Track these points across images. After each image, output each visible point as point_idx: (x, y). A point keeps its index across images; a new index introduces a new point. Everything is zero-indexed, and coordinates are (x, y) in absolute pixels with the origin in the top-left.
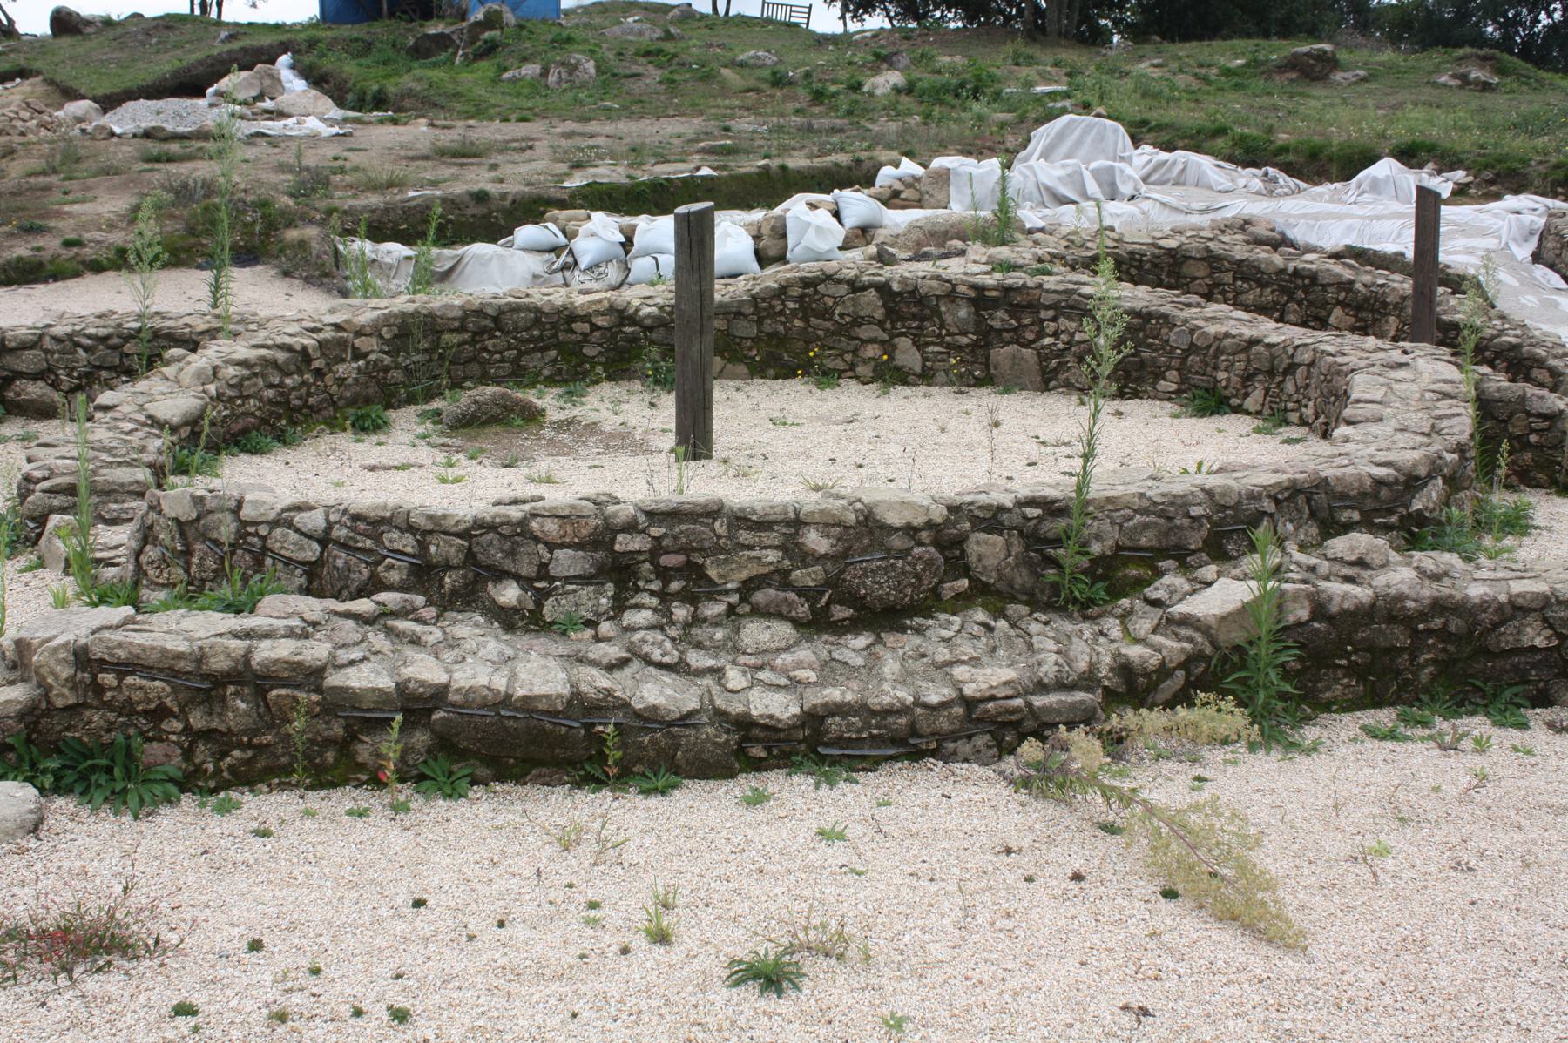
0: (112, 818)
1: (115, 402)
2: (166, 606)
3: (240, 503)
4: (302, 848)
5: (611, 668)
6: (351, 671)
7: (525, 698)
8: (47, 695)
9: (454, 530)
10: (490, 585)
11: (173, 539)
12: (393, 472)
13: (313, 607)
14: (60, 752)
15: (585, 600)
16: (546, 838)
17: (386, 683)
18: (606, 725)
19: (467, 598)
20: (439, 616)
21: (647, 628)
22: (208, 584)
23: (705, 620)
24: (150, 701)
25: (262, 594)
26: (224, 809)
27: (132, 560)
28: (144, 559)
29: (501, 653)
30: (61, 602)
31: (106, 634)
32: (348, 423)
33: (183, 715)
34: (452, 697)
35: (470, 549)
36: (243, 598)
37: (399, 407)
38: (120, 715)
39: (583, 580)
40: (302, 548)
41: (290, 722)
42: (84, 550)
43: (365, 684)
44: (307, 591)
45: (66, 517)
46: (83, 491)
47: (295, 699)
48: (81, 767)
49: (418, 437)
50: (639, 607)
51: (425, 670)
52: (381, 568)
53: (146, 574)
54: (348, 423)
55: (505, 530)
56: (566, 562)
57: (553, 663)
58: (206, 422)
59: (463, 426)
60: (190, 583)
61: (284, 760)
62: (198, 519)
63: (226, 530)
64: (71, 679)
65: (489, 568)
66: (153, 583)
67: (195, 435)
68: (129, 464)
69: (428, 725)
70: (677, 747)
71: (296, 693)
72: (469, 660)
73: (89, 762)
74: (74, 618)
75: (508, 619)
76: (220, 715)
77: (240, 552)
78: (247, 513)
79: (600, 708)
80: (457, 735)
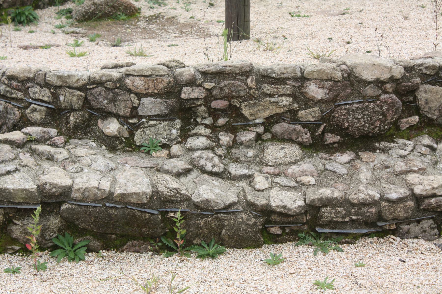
5: (178, 175)
6: (7, 178)
7: (122, 195)
9: (75, 85)
10: (100, 121)
12: (39, 50)
15: (162, 131)
16: (135, 287)
17: (31, 186)
18: (175, 212)
19: (85, 129)
20: (66, 142)
21: (203, 149)
23: (241, 144)
29: (107, 166)
34: (74, 195)
35: (86, 98)
37: (44, 8)
39: (161, 117)
49: (57, 27)
50: (197, 135)
51: (56, 177)
52: (28, 111)
55: (109, 85)
57: (140, 172)
59: (86, 20)
69: (58, 213)
70: (222, 227)
72: (86, 170)
75: (111, 144)
79: (172, 201)
80: (78, 219)
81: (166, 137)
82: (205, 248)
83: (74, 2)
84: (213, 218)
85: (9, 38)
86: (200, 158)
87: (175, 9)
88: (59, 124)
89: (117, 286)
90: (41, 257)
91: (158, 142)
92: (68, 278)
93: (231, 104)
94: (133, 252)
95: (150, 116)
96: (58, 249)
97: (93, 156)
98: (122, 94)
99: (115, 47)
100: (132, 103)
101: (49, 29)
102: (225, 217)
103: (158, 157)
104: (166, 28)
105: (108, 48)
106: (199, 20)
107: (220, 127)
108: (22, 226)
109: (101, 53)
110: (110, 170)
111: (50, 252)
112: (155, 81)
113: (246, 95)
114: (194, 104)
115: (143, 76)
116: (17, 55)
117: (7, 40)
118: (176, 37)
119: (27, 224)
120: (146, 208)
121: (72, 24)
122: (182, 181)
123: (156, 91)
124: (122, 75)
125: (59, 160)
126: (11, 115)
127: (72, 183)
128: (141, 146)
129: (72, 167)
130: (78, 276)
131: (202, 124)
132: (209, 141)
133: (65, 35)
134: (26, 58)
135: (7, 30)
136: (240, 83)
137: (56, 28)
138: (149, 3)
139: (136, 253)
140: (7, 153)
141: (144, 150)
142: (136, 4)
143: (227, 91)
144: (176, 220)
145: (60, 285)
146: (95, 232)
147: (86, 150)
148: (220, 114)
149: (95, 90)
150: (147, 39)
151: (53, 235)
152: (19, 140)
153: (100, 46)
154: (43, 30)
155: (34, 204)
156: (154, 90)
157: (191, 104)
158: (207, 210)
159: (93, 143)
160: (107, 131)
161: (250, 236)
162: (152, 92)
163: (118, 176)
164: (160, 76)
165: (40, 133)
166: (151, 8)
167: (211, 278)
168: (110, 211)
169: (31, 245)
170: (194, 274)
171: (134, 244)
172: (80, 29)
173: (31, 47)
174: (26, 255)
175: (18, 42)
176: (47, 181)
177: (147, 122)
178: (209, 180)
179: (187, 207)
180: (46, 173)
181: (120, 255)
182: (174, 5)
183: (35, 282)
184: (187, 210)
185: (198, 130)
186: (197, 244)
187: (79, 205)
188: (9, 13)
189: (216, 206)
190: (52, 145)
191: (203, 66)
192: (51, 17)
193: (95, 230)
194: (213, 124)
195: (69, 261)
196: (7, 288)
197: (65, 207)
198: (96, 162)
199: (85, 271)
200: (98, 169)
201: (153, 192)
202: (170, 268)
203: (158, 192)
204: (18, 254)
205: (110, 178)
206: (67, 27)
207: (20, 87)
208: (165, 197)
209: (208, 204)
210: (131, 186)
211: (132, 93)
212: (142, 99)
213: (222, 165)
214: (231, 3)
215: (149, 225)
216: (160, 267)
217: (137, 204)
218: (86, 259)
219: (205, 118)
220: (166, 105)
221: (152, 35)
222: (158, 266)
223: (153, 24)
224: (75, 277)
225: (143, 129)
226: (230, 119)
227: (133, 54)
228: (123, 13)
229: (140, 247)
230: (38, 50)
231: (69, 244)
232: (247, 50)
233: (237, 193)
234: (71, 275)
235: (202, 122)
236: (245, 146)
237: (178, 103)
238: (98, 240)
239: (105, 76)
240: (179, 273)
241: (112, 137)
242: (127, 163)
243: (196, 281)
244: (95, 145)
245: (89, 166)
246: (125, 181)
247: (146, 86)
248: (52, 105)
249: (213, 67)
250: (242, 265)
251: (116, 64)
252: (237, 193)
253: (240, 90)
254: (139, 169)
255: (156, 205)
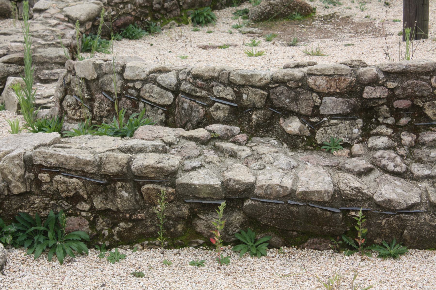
0: (47, 263)
1: (46, 7)
2: (78, 133)
3: (123, 68)
4: (162, 285)
5: (360, 174)
6: (193, 173)
7: (304, 193)
8: (8, 186)
9: (258, 84)
10: (281, 120)
11: (83, 91)
12: (218, 50)
13: (169, 133)
14: (16, 221)
15: (343, 130)
16: (317, 284)
17: (215, 181)
18: (356, 211)
19: (267, 128)
20: (248, 140)
21: (384, 149)
22: (104, 119)
23: (424, 144)
24: (70, 191)
25: (138, 125)
26: (115, 259)
27: (58, 104)
28: (65, 104)
29: (289, 163)
30: (16, 130)
31: (43, 149)
32: (190, 18)
33: (89, 200)
34: (257, 191)
35: (268, 97)
36: (126, 127)
37: (221, 9)
38: (52, 199)
39: (343, 117)
40: (162, 96)
41: (155, 205)
42: (29, 98)
43: (202, 182)
44: (165, 124)
45: (18, 79)
46: (28, 61)
47: (159, 191)
48: (28, 231)
49: (233, 27)
50: (379, 134)
51: (240, 174)
52: (212, 109)
53: (66, 113)
54: (190, 18)
55: (292, 84)
56: (331, 105)
57: (322, 171)
58: (102, 19)
59: (262, 20)
60: (93, 119)
61: (151, 229)
62: (98, 78)
63: (115, 86)
64: (22, 177)
65: (280, 109)
66: (71, 118)
67: (95, 27)
68: (55, 45)
69: (241, 209)
70: (404, 227)
71: (159, 187)
72: (268, 168)
73: (33, 228)
74: (24, 140)
75: (293, 142)
76: (112, 200)
77: (124, 99)
78: (128, 74)
79: (353, 200)
80: (260, 216)
81: (347, 136)
82: (386, 248)
83: (250, 2)
84: (395, 218)
85: (189, 38)
86: (382, 157)
87: (350, 9)
88: (242, 122)
89: (298, 282)
90: (224, 251)
91: (339, 141)
92: (250, 273)
93: (414, 104)
94: (314, 249)
95: (331, 115)
96: (240, 244)
97: (275, 153)
98: (304, 93)
99: (292, 47)
100: (314, 102)
101: (226, 29)
102: (407, 217)
103: (339, 156)
104: (341, 27)
105: (284, 47)
106: (375, 20)
107: (402, 127)
108: (206, 221)
109: (278, 53)
110: (292, 167)
111: (232, 247)
112: (337, 81)
113: (430, 95)
114: (376, 103)
115: (325, 75)
116: (197, 54)
117: (186, 40)
118: (351, 36)
119: (211, 219)
120: (328, 207)
121: (249, 25)
122: (363, 180)
123: (338, 91)
124: (305, 74)
125: (242, 158)
126: (195, 113)
127: (255, 180)
128: (322, 145)
129: (255, 164)
130: (260, 271)
131: (384, 124)
132: (391, 141)
133: (241, 35)
134: (206, 57)
135: (186, 31)
136: (423, 83)
137: (233, 28)
138: (324, 3)
139: (317, 251)
140: (192, 149)
141: (325, 149)
142: (311, 4)
143: (410, 90)
144: (357, 219)
145: (243, 280)
146: (276, 228)
147: (268, 148)
148: (402, 114)
149: (277, 89)
150: (322, 38)
151: (235, 231)
152: (203, 137)
153: (277, 46)
154: (221, 30)
155: (218, 200)
156: (336, 89)
157: (373, 103)
158: (389, 210)
159: (275, 141)
160: (289, 130)
161: (433, 238)
162: (334, 92)
163: (300, 174)
164: (343, 75)
165: (224, 130)
166: (326, 8)
167: (394, 278)
168: (292, 208)
169: (215, 239)
170: (376, 273)
171: (315, 242)
172: (256, 29)
173: (210, 47)
174: (210, 249)
175: (197, 41)
176: (231, 177)
177: (329, 121)
178: (390, 180)
179: (369, 206)
180: (230, 170)
181: (300, 252)
182: (348, 5)
183: (219, 275)
184: (369, 209)
185: (380, 130)
186: (378, 244)
187: (261, 202)
188: (188, 14)
189: (398, 206)
190: (235, 142)
191: (386, 66)
192: (228, 17)
193: (277, 227)
194: (395, 123)
195: (252, 257)
196: (193, 280)
197: (248, 203)
198: (278, 159)
199: (267, 267)
200: (280, 167)
201: (335, 190)
202: (351, 267)
203: (339, 191)
204: (202, 247)
205: (292, 176)
206: (244, 27)
207: (204, 86)
208: (347, 195)
209: (390, 203)
210: (313, 184)
211: (314, 92)
212: (324, 98)
213: (404, 165)
214: (409, 1)
215: (330, 223)
216: (341, 266)
217: (319, 202)
218: (268, 255)
219: (387, 118)
220: (348, 104)
221: (326, 34)
222: (339, 264)
223: (328, 24)
224: (257, 272)
225: (324, 128)
226: (412, 119)
227: (310, 53)
228: (298, 13)
229: (320, 244)
230: (217, 49)
231: (251, 239)
232: (425, 49)
233: (419, 194)
234: (253, 270)
235: (384, 122)
236: (428, 147)
237: (360, 102)
238: (280, 236)
239: (288, 76)
240: (361, 272)
241: (294, 135)
242: (308, 162)
243: (378, 280)
244: (276, 143)
245: (271, 164)
246: (307, 179)
247: (328, 86)
248: (235, 103)
249: (396, 67)
250: (425, 266)
251: (298, 64)
252: (419, 194)
253: (424, 90)
254: (320, 167)
255: (337, 203)
